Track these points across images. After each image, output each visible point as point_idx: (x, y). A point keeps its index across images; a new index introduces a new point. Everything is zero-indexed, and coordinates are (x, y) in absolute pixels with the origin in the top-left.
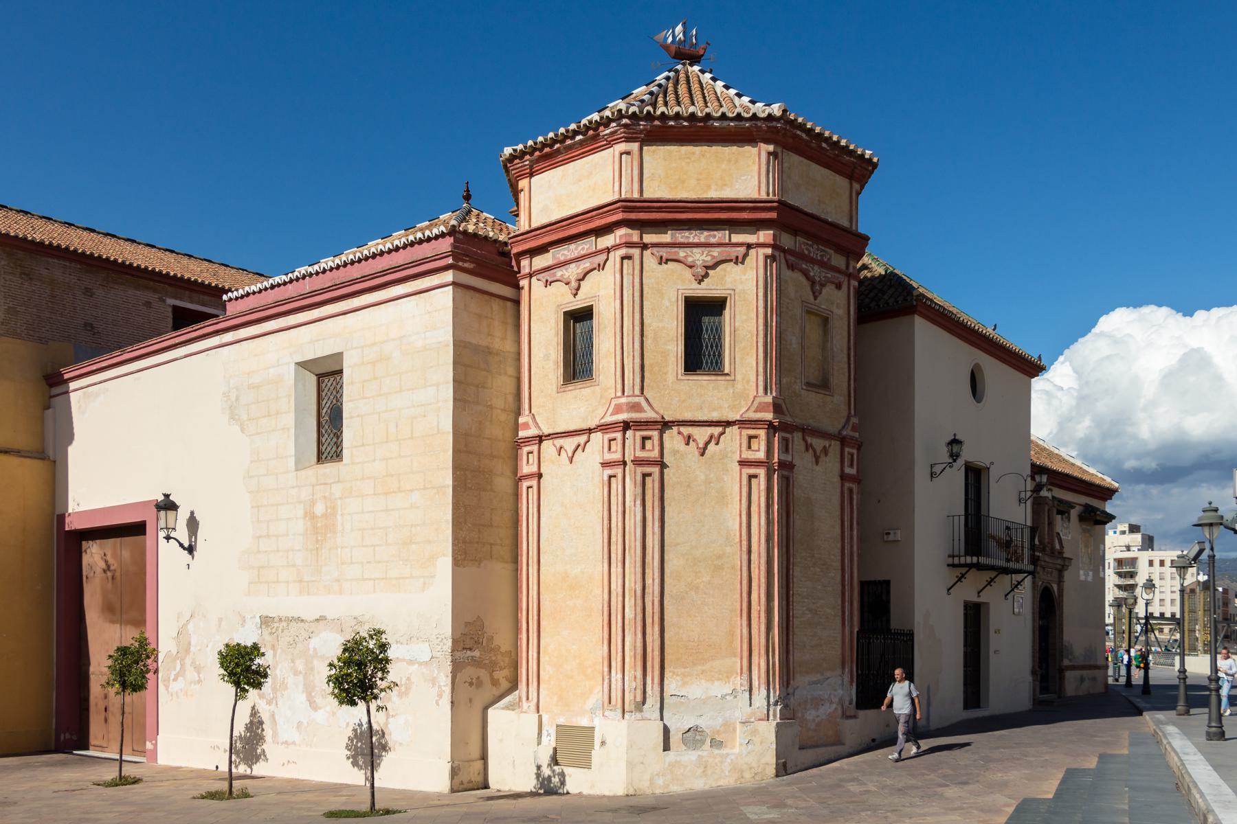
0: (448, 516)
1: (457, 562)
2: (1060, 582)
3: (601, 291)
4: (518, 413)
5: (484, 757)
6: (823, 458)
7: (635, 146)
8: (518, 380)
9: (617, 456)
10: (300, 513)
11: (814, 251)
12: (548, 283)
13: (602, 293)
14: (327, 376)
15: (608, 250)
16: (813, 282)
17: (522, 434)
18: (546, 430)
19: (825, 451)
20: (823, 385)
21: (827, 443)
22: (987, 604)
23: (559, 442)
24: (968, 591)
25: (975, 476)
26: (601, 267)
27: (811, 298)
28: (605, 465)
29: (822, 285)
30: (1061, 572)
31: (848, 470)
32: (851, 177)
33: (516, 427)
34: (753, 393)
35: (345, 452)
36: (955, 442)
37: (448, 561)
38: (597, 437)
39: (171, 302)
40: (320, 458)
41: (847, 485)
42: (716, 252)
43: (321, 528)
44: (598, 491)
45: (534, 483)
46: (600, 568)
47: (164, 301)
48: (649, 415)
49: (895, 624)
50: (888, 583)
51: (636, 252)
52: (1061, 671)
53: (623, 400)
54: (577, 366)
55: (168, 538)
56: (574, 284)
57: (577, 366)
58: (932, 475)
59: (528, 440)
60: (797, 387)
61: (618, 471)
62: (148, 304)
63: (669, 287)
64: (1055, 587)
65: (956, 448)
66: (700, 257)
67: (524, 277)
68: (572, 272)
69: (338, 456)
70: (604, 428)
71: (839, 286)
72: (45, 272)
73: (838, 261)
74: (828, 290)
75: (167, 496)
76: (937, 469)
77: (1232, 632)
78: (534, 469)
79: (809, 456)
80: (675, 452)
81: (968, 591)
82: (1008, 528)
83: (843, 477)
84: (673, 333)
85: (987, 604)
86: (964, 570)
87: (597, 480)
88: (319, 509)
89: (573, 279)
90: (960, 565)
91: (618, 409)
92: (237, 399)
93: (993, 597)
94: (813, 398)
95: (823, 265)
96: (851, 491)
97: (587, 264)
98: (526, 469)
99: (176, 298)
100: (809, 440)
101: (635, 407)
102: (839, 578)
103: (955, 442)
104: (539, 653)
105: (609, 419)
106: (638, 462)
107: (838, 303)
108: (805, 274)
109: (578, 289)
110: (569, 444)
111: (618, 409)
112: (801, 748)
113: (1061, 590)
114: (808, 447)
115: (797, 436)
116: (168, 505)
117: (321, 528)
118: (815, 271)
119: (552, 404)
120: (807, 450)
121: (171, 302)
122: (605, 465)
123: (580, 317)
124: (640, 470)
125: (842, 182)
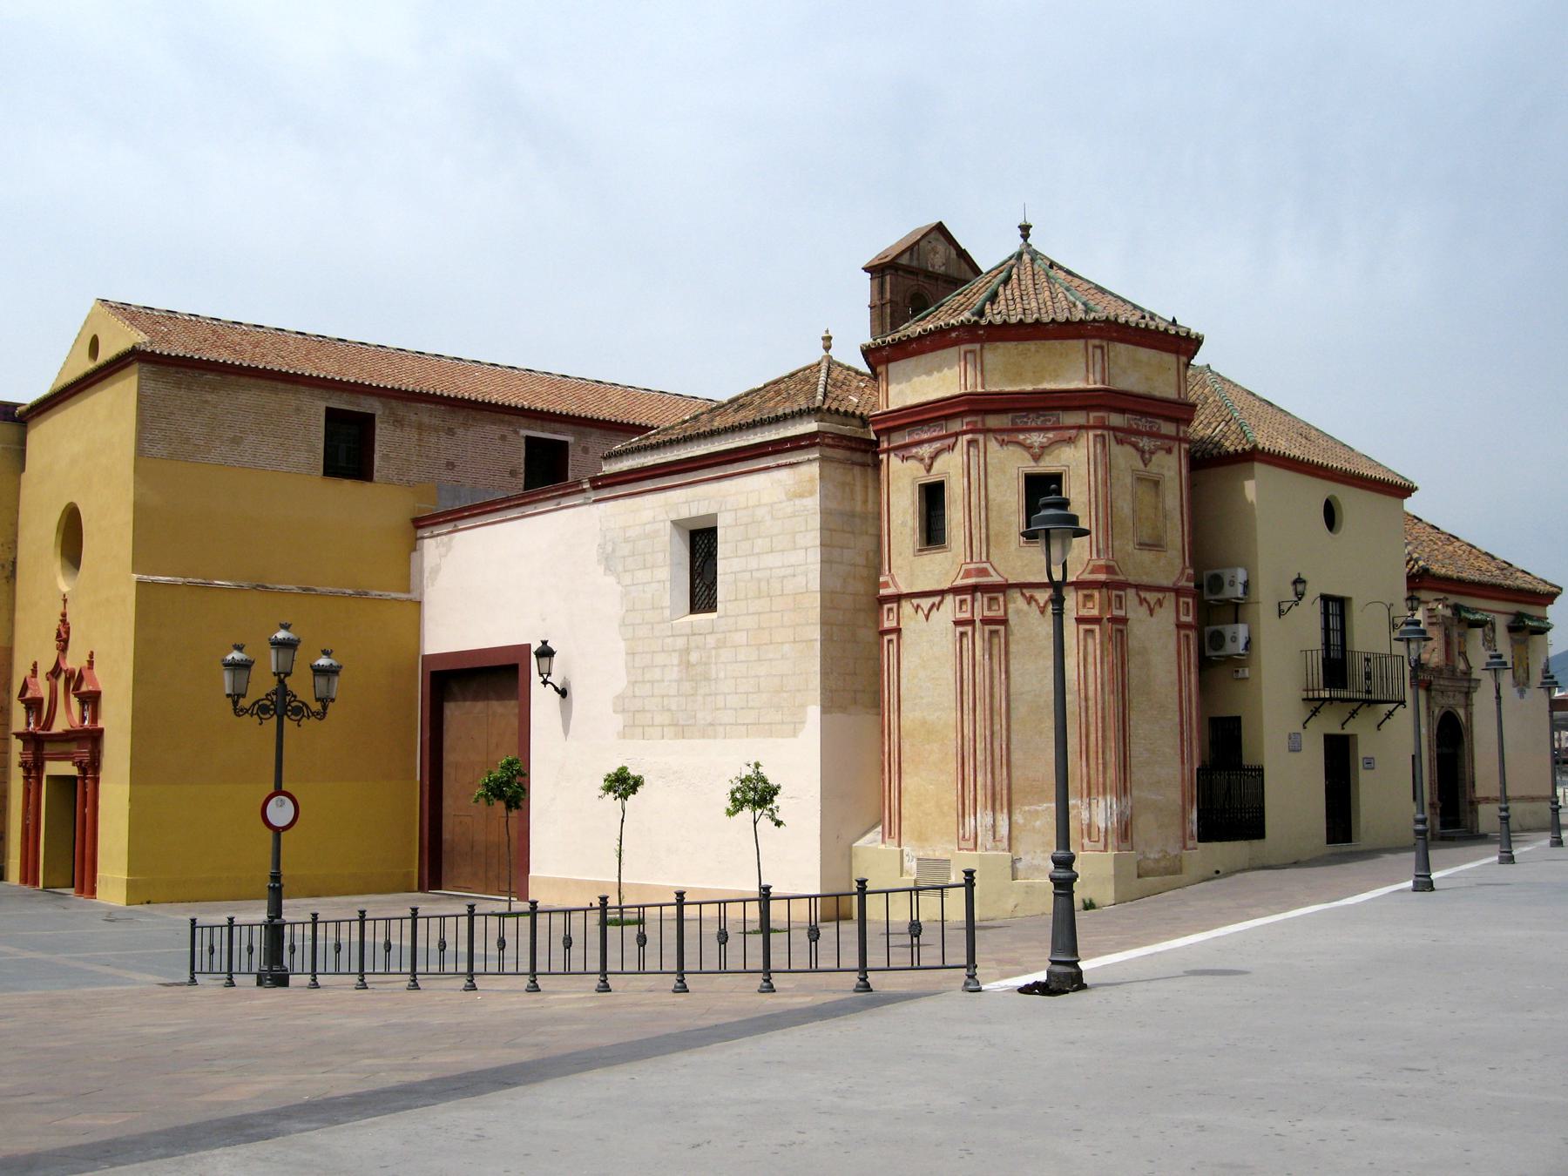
0: (818, 668)
1: (825, 710)
2: (1468, 705)
3: (951, 467)
4: (879, 572)
5: (1124, 301)
6: (1157, 609)
7: (977, 346)
8: (879, 537)
9: (967, 615)
10: (676, 661)
11: (1143, 424)
12: (904, 459)
13: (952, 472)
14: (702, 543)
15: (956, 435)
16: (1142, 452)
17: (883, 592)
18: (905, 590)
19: (1160, 603)
20: (1154, 545)
21: (1160, 596)
22: (1355, 736)
23: (915, 601)
24: (1329, 723)
25: (1335, 608)
26: (951, 448)
27: (1141, 466)
28: (957, 623)
29: (1152, 453)
30: (1468, 695)
31: (1184, 619)
32: (1177, 352)
33: (878, 585)
34: (1086, 556)
35: (719, 606)
36: (1299, 581)
37: (818, 709)
38: (949, 598)
39: (524, 433)
40: (694, 609)
41: (1182, 632)
42: (1051, 435)
43: (694, 673)
44: (951, 646)
45: (894, 637)
46: (952, 716)
47: (517, 433)
48: (995, 579)
49: (1248, 760)
50: (1239, 719)
51: (981, 438)
52: (1473, 804)
53: (972, 566)
54: (933, 533)
55: (545, 682)
56: (927, 461)
57: (933, 533)
58: (1281, 613)
59: (890, 631)
60: (1130, 547)
61: (969, 629)
62: (503, 438)
63: (1008, 468)
64: (1461, 712)
65: (1300, 587)
66: (1036, 439)
67: (883, 452)
68: (926, 451)
69: (711, 606)
70: (955, 591)
71: (1169, 451)
72: (414, 418)
73: (1168, 428)
74: (1160, 457)
75: (544, 643)
76: (1285, 607)
77: (1567, 763)
78: (894, 624)
79: (1144, 610)
80: (1018, 612)
81: (1329, 723)
82: (1368, 660)
83: (1180, 626)
84: (1014, 506)
85: (1355, 736)
86: (1317, 704)
87: (950, 636)
88: (694, 657)
89: (926, 456)
90: (1314, 699)
91: (968, 574)
92: (614, 551)
93: (1361, 729)
94: (1147, 556)
95: (1151, 435)
96: (1187, 637)
97: (937, 445)
98: (887, 625)
99: (529, 428)
100: (1143, 594)
101: (983, 572)
102: (1177, 719)
103: (1299, 581)
104: (1008, 677)
105: (960, 582)
106: (985, 621)
107: (1171, 468)
108: (1135, 446)
109: (931, 465)
110: (926, 603)
111: (968, 574)
112: (1139, 876)
113: (1469, 716)
114: (1142, 601)
115: (1131, 593)
116: (546, 653)
117: (694, 673)
118: (1144, 443)
119: (910, 568)
120: (1141, 603)
121: (524, 433)
122: (957, 623)
123: (933, 496)
124: (987, 628)
125: (1169, 359)
